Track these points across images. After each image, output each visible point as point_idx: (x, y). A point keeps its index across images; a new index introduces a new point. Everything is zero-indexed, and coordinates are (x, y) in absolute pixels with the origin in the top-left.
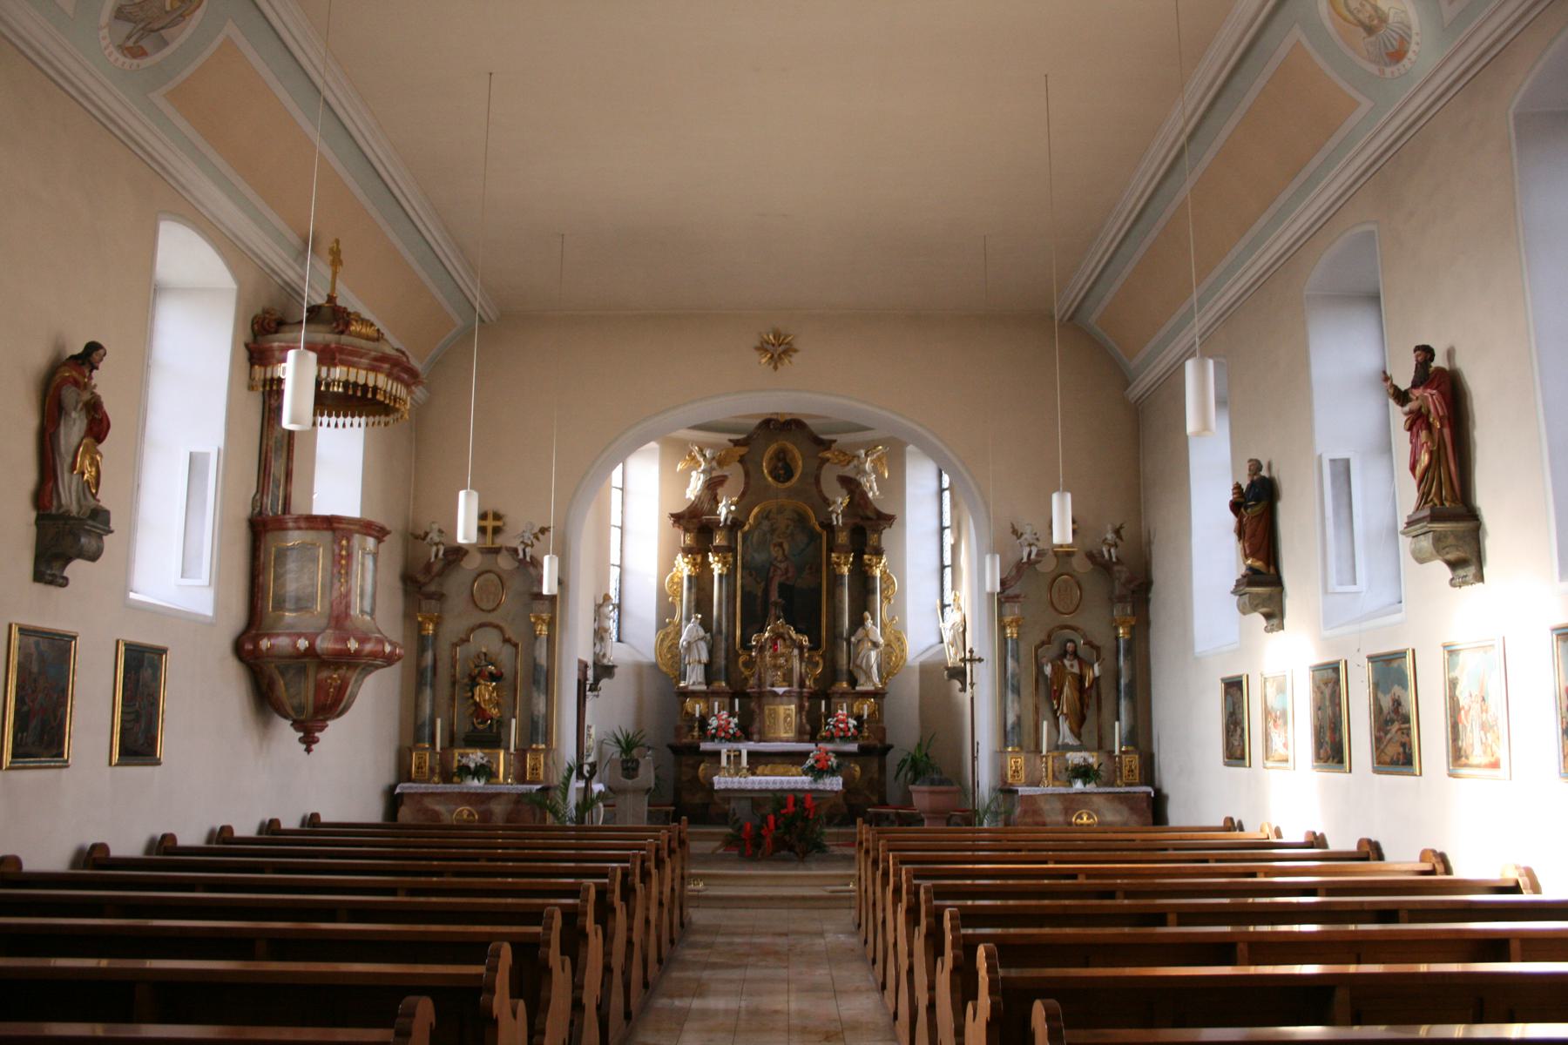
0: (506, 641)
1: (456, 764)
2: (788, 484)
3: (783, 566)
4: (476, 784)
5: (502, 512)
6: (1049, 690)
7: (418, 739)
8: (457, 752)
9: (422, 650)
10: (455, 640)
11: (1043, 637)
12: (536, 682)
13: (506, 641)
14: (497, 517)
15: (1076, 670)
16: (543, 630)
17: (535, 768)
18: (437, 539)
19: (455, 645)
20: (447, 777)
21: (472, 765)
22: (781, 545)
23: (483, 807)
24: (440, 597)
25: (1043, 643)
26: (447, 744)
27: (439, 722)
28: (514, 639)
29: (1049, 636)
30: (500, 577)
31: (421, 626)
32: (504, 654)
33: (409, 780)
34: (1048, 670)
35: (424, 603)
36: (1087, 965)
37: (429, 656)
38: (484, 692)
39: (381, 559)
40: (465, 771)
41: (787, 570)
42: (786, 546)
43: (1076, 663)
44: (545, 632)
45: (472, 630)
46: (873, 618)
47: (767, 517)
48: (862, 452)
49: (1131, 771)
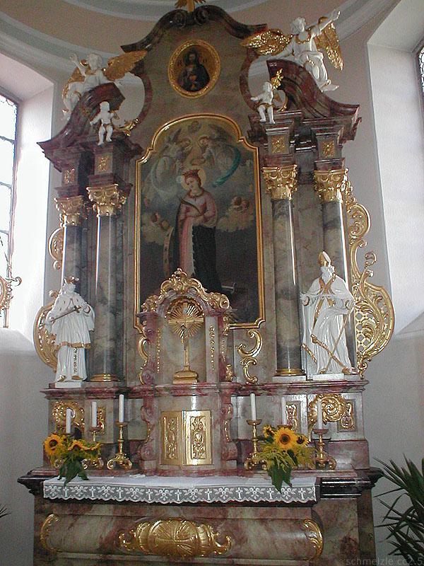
2: (202, 93)
3: (198, 202)
22: (195, 174)
36: (339, 217)
41: (205, 208)
42: (202, 174)
46: (336, 261)
47: (176, 140)
48: (301, 24)
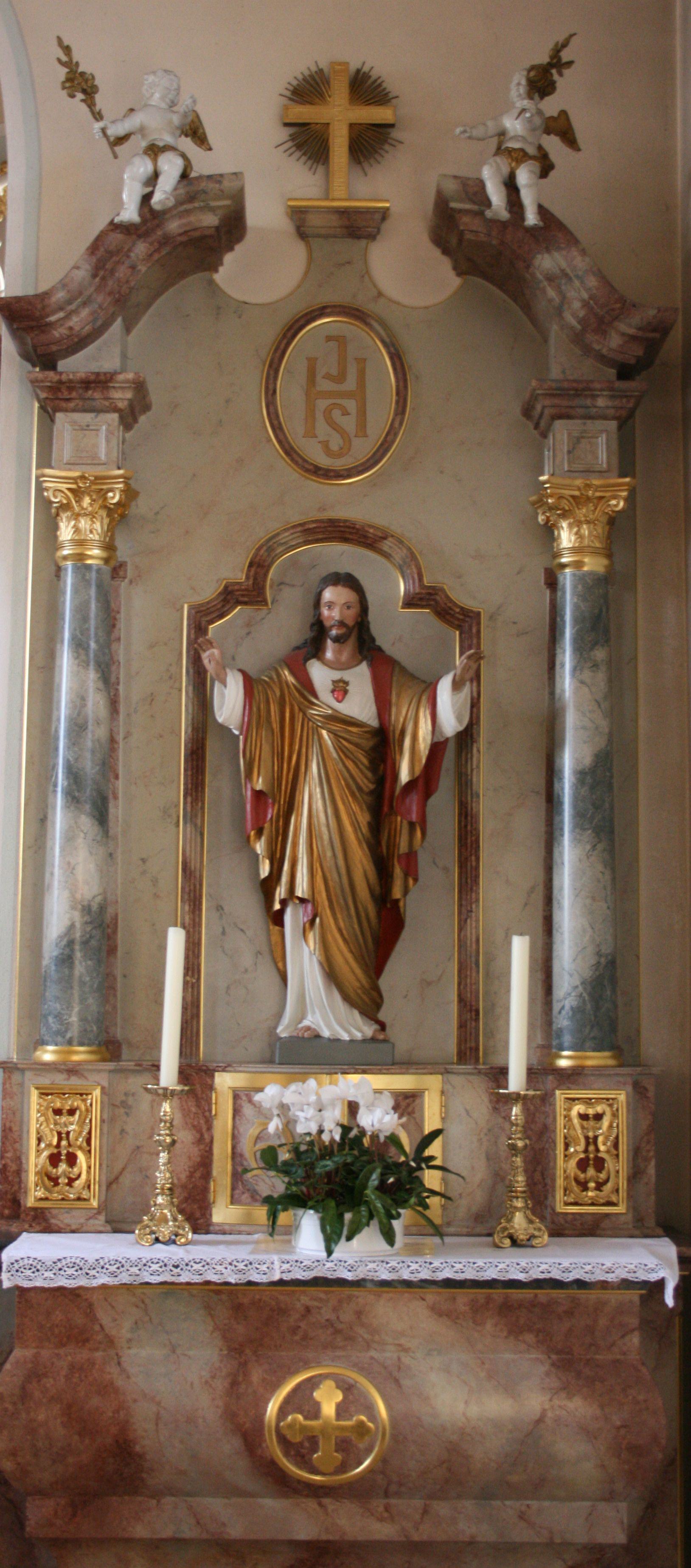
6: (234, 785)
11: (235, 571)
14: (365, 88)
15: (360, 705)
25: (230, 597)
29: (258, 566)
34: (229, 703)
43: (360, 678)
49: (592, 1161)
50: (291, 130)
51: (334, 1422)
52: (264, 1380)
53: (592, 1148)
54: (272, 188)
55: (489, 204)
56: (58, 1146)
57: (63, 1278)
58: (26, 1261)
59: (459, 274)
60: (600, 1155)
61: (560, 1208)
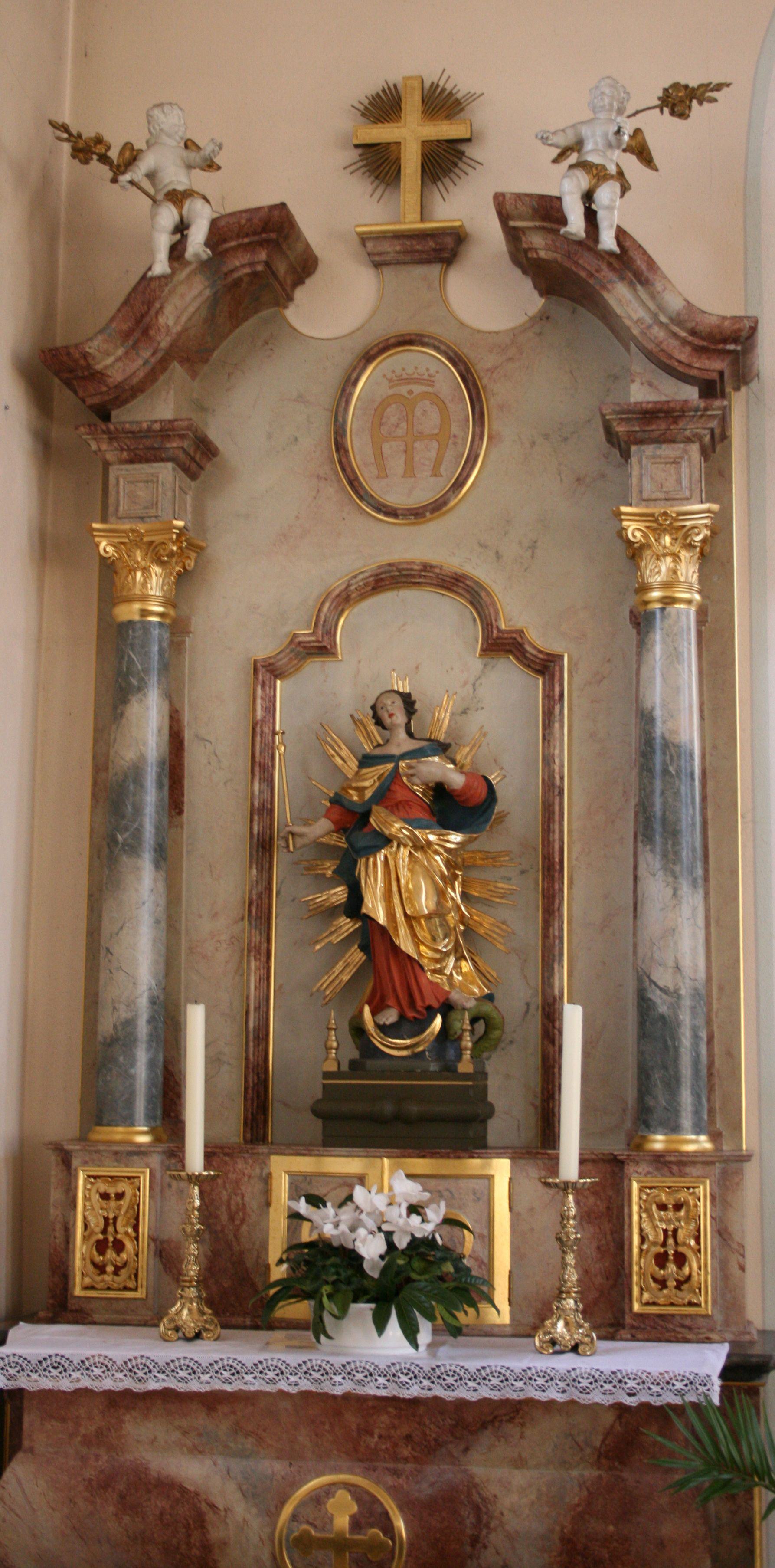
0: (502, 644)
1: (275, 1249)
4: (376, 1351)
5: (462, 82)
7: (100, 1105)
8: (283, 1168)
9: (116, 691)
10: (265, 650)
12: (652, 826)
13: (502, 644)
14: (441, 102)
16: (673, 573)
17: (670, 1255)
18: (176, 177)
19: (268, 671)
20: (239, 1300)
21: (371, 1249)
23: (436, 1476)
24: (198, 456)
26: (233, 1129)
27: (196, 1019)
28: (539, 639)
30: (456, 359)
31: (110, 580)
32: (486, 718)
33: (62, 1308)
35: (123, 476)
37: (147, 719)
38: (407, 880)
39: (120, 925)
40: (329, 1275)
44: (689, 594)
45: (345, 599)
50: (360, 151)
51: (348, 1536)
52: (90, 1480)
53: (111, 1229)
54: (333, 210)
55: (564, 221)
56: (664, 1244)
57: (671, 1394)
58: (139, 1361)
59: (541, 294)
60: (119, 1236)
61: (78, 1292)
